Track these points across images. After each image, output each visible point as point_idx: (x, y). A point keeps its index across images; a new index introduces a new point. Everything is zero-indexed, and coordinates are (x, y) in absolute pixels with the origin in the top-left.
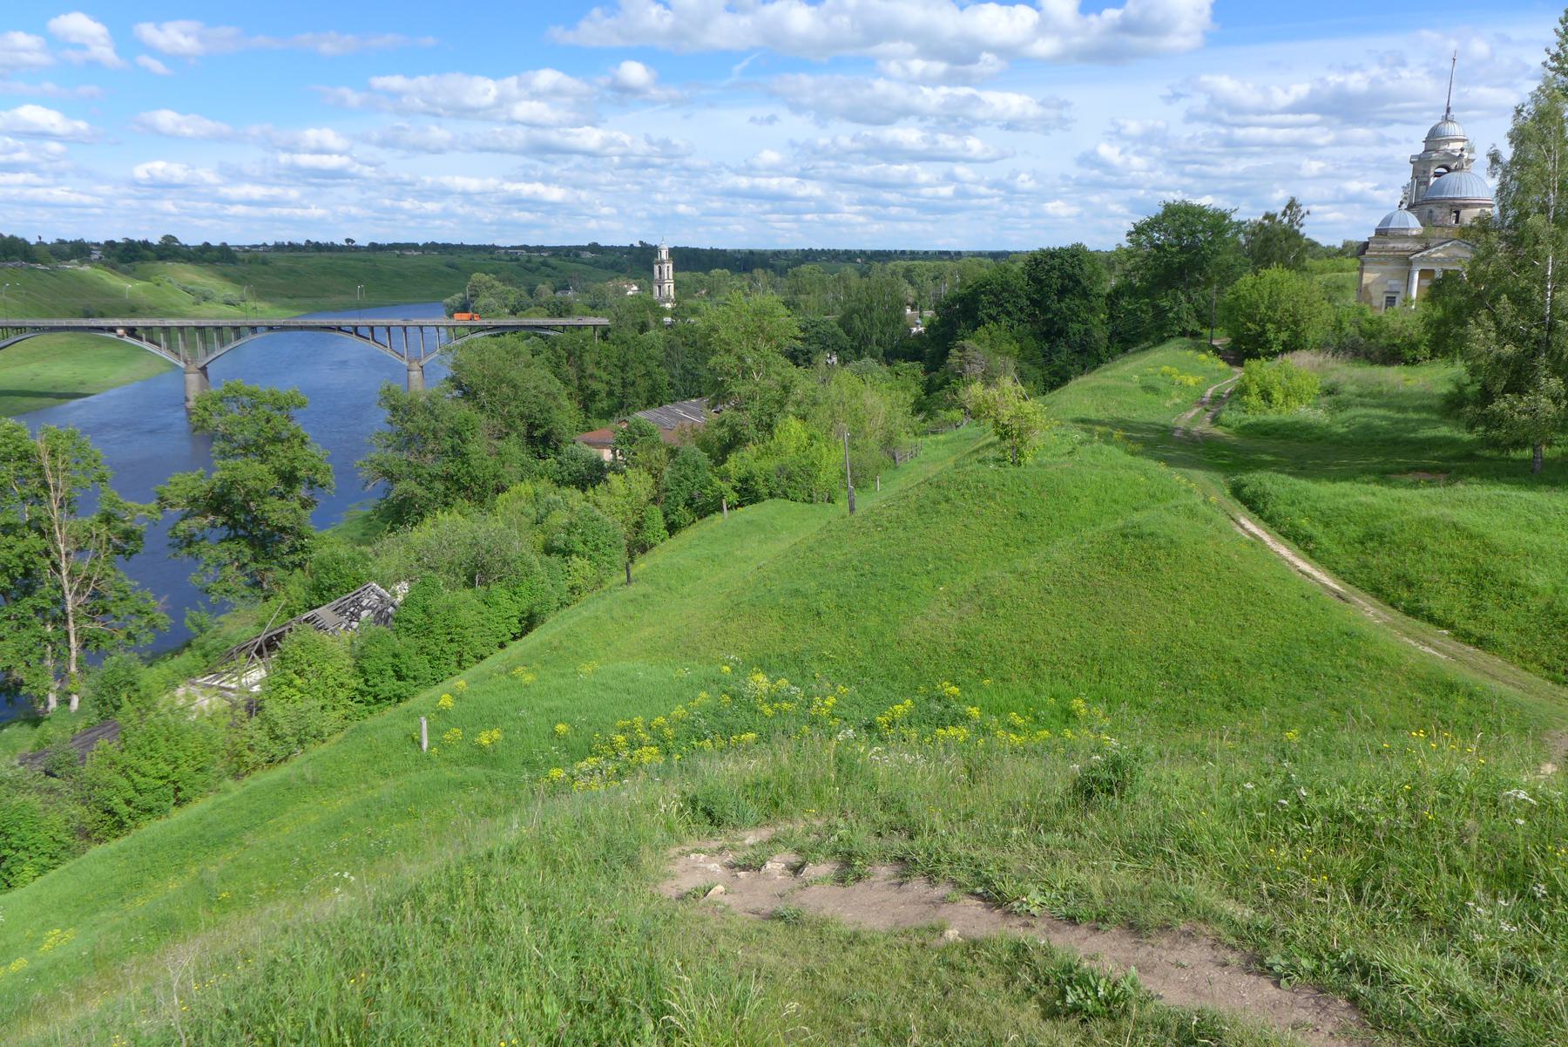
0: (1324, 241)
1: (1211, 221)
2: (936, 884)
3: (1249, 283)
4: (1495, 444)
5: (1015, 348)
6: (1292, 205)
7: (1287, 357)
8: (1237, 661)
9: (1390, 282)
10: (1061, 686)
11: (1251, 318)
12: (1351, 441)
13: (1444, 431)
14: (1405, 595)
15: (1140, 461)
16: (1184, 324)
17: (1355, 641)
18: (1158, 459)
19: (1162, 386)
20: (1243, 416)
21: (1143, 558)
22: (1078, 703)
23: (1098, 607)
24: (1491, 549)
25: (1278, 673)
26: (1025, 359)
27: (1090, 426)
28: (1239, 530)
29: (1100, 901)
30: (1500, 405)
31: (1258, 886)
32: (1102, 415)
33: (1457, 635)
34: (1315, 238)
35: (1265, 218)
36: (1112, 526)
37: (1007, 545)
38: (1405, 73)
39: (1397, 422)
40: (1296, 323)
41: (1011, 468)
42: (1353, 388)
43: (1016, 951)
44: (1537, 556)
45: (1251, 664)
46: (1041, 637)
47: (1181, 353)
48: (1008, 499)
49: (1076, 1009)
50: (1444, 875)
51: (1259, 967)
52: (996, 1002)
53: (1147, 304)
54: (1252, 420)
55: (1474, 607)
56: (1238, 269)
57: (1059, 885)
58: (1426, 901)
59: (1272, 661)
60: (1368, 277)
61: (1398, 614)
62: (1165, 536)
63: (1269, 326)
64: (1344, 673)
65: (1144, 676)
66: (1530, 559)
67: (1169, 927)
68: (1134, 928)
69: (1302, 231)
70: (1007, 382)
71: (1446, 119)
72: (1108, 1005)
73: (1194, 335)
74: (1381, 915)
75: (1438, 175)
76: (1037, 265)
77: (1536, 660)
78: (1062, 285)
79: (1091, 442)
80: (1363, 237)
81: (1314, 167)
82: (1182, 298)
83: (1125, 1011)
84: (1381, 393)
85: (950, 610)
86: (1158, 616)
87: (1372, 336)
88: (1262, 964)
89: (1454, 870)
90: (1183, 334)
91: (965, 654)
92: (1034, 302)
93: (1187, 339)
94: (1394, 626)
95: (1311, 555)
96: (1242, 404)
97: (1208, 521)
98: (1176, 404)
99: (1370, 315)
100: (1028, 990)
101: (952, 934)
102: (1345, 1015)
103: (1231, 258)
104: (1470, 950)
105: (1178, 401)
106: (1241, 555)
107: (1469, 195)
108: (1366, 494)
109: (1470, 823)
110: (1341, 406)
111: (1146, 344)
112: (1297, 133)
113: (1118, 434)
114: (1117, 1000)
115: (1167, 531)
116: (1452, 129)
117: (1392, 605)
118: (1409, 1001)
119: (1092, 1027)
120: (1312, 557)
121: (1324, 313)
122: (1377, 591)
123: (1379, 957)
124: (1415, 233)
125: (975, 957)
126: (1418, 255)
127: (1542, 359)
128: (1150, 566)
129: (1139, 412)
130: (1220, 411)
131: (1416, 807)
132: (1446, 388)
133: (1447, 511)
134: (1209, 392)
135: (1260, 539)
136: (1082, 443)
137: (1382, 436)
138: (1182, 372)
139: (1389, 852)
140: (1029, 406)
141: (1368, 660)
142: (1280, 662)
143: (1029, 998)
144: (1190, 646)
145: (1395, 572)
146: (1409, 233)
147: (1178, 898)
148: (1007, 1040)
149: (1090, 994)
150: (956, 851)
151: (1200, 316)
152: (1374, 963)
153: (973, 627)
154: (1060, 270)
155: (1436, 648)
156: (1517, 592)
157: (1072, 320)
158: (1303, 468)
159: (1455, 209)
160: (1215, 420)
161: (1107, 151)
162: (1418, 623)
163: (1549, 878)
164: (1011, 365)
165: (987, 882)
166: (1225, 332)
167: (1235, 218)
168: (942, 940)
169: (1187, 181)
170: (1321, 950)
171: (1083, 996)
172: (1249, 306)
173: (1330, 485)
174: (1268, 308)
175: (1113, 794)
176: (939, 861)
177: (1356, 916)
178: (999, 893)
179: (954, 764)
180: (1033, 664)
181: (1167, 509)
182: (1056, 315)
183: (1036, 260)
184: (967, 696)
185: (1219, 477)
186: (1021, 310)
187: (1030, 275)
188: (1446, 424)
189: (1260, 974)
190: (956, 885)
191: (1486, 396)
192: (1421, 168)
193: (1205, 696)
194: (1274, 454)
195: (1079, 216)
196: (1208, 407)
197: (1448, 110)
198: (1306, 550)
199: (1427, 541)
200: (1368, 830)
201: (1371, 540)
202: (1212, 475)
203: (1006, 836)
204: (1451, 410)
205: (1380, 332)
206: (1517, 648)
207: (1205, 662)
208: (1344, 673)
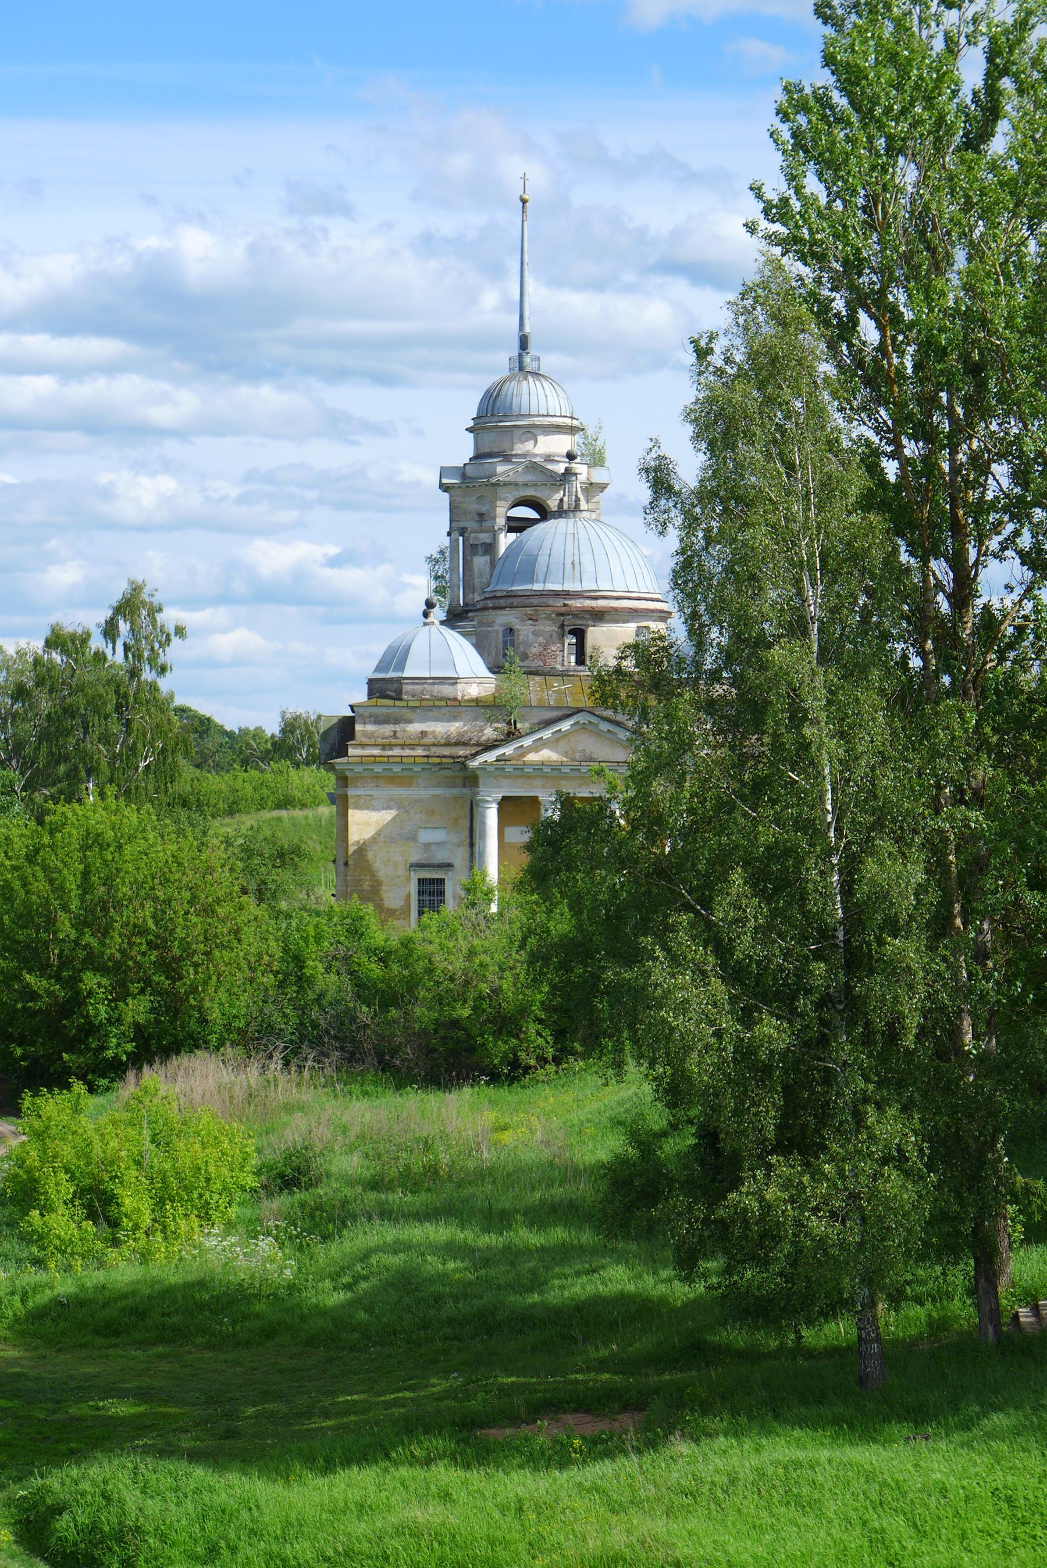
7: (153, 1077)
9: (426, 836)
20: (32, 1276)
34: (203, 707)
35: (49, 644)
38: (339, 231)
39: (485, 1259)
40: (171, 968)
54: (64, 1287)
63: (90, 980)
69: (164, 684)
75: (517, 526)
84: (432, 1171)
96: (26, 1239)
99: (378, 936)
107: (604, 585)
108: (423, 1499)
121: (249, 934)
124: (474, 691)
126: (491, 757)
127: (843, 1047)
137: (449, 1308)
158: (232, 1434)
159: (570, 622)
172: (25, 919)
174: (80, 924)
188: (621, 1258)
192: (471, 505)
194: (142, 1395)
197: (524, 343)
205: (412, 984)
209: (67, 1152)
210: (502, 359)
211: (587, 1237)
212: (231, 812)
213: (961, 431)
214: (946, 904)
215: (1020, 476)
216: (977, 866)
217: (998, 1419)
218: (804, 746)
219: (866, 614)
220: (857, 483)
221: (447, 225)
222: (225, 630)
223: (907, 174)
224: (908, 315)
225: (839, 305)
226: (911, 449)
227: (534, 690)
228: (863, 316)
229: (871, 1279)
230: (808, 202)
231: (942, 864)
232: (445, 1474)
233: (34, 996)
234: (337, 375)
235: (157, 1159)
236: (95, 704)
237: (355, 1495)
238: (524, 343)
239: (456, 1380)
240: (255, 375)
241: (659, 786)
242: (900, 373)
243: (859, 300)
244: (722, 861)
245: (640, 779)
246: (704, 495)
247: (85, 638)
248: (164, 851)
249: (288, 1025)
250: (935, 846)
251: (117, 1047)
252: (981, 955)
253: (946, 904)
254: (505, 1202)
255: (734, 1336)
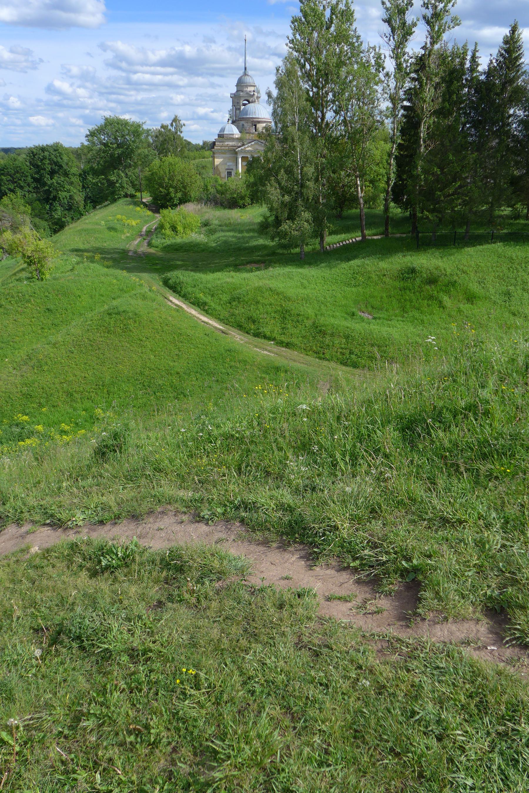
0: (194, 142)
1: (133, 129)
2: (22, 525)
3: (158, 165)
4: (284, 247)
5: (29, 209)
6: (175, 120)
7: (182, 206)
8: (178, 373)
9: (228, 164)
10: (88, 404)
11: (161, 185)
12: (219, 250)
13: (261, 241)
14: (252, 327)
15: (112, 271)
16: (125, 190)
17: (233, 354)
18: (122, 269)
19: (118, 227)
20: (163, 241)
21: (122, 325)
22: (99, 411)
23: (101, 356)
24: (288, 299)
25: (198, 376)
26: (36, 216)
27: (81, 253)
28: (170, 303)
29: (115, 509)
30: (285, 227)
31: (193, 479)
32: (87, 246)
33: (277, 343)
34: (189, 140)
35: (161, 127)
36: (102, 310)
37: (42, 328)
38: (213, 46)
39: (239, 238)
40: (184, 187)
41: (38, 283)
42: (216, 222)
43: (72, 548)
44: (306, 299)
45: (185, 373)
46: (72, 378)
47: (126, 207)
48: (38, 301)
49: (107, 567)
50: (276, 452)
51: (198, 519)
52: (63, 578)
53: (103, 179)
54: (169, 243)
55: (283, 328)
56: (150, 158)
57: (92, 507)
58: (270, 466)
59: (195, 370)
60: (217, 161)
61: (250, 337)
62: (132, 312)
63: (171, 190)
64: (230, 371)
65: (131, 390)
66: (304, 302)
67: (152, 512)
68: (135, 517)
69: (182, 135)
70: (27, 230)
71: (245, 74)
72: (124, 560)
73: (132, 196)
74: (251, 478)
75: (244, 105)
76: (34, 156)
77: (311, 350)
78: (51, 169)
79: (83, 263)
80: (212, 138)
81: (179, 98)
82: (123, 175)
83: (134, 560)
84: (230, 223)
85: (15, 372)
86: (134, 356)
87: (222, 193)
88: (199, 517)
89: (280, 449)
90: (126, 196)
91: (28, 396)
92: (36, 180)
93: (129, 199)
94: (249, 343)
95: (207, 312)
96: (162, 234)
97: (153, 300)
98: (127, 237)
99: (220, 182)
100: (81, 566)
101: (35, 549)
102: (239, 529)
103: (146, 151)
104: (290, 482)
105: (128, 235)
106: (172, 317)
107: (260, 116)
108: (229, 277)
109: (285, 425)
110: (212, 232)
111: (106, 203)
112: (168, 78)
113: (98, 257)
114: (128, 556)
115: (132, 309)
116: (248, 80)
117: (247, 333)
118: (266, 514)
119: (117, 574)
120: (207, 314)
121: (198, 181)
122: (240, 327)
123: (251, 498)
124: (237, 136)
125: (49, 558)
126: (240, 149)
127: (300, 202)
128: (126, 329)
129: (108, 243)
130: (152, 239)
131: (262, 424)
132: (259, 219)
133: (267, 282)
134: (144, 229)
135: (181, 307)
136: (78, 263)
137: (233, 247)
138: (128, 218)
139: (252, 447)
140: (42, 244)
141: (240, 362)
142: (199, 370)
143: (81, 570)
144: (153, 369)
145: (247, 316)
146: (234, 136)
147: (155, 496)
148: (71, 596)
149: (114, 557)
150: (31, 504)
151: (134, 186)
152: (249, 501)
153: (30, 379)
154: (49, 160)
155: (269, 351)
156: (300, 318)
157: (61, 190)
158: (197, 267)
159: (254, 123)
160: (150, 245)
161: (64, 86)
162: (259, 340)
163: (319, 443)
164: (28, 220)
165: (52, 516)
166: (149, 194)
167: (145, 127)
168: (29, 554)
169: (112, 105)
170: (226, 502)
171: (110, 560)
172: (160, 178)
173: (212, 275)
174: (169, 179)
175: (116, 451)
176: (22, 512)
177: (240, 482)
178: (59, 520)
179: (27, 457)
180: (69, 394)
181: (130, 297)
182: (50, 187)
183: (33, 153)
184: (34, 420)
185: (156, 276)
186: (29, 185)
187: (30, 162)
188: (261, 238)
189: (198, 522)
190: (34, 522)
191: (278, 222)
192: (236, 101)
193: (165, 395)
194: (182, 261)
195: (53, 125)
196: (145, 237)
197: (245, 69)
198: (204, 310)
199: (259, 298)
200: (241, 440)
201: (234, 301)
202: (152, 275)
203: (59, 488)
204: (263, 230)
205: (226, 190)
206: (303, 345)
207: (162, 377)
208: (230, 371)
209: (168, 220)
210: (241, 72)
211: (256, 235)
212: (194, 159)
213: (324, 87)
214: (318, 176)
215: (334, 96)
216: (323, 169)
217: (323, 265)
218: (294, 147)
219: (306, 122)
220: (305, 96)
221: (233, 45)
222: (193, 125)
223: (315, 35)
224: (314, 63)
225: (302, 61)
226: (315, 90)
227: (247, 136)
228: (306, 63)
229: (303, 241)
230: (297, 40)
231: (318, 168)
232: (232, 273)
233: (161, 192)
234: (212, 75)
235: (184, 221)
236: (170, 138)
237: (218, 277)
238: (245, 69)
239: (233, 259)
240: (198, 75)
241: (269, 154)
242: (313, 75)
243: (306, 60)
244: (280, 168)
245: (266, 152)
246: (278, 98)
247: (168, 126)
248: (182, 166)
249: (205, 198)
250: (316, 165)
251: (176, 202)
252: (323, 185)
253: (318, 176)
254: (242, 229)
255: (280, 251)
